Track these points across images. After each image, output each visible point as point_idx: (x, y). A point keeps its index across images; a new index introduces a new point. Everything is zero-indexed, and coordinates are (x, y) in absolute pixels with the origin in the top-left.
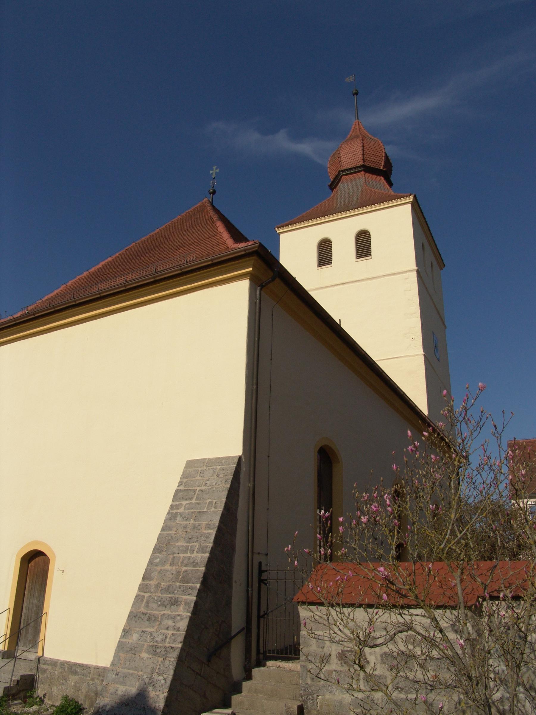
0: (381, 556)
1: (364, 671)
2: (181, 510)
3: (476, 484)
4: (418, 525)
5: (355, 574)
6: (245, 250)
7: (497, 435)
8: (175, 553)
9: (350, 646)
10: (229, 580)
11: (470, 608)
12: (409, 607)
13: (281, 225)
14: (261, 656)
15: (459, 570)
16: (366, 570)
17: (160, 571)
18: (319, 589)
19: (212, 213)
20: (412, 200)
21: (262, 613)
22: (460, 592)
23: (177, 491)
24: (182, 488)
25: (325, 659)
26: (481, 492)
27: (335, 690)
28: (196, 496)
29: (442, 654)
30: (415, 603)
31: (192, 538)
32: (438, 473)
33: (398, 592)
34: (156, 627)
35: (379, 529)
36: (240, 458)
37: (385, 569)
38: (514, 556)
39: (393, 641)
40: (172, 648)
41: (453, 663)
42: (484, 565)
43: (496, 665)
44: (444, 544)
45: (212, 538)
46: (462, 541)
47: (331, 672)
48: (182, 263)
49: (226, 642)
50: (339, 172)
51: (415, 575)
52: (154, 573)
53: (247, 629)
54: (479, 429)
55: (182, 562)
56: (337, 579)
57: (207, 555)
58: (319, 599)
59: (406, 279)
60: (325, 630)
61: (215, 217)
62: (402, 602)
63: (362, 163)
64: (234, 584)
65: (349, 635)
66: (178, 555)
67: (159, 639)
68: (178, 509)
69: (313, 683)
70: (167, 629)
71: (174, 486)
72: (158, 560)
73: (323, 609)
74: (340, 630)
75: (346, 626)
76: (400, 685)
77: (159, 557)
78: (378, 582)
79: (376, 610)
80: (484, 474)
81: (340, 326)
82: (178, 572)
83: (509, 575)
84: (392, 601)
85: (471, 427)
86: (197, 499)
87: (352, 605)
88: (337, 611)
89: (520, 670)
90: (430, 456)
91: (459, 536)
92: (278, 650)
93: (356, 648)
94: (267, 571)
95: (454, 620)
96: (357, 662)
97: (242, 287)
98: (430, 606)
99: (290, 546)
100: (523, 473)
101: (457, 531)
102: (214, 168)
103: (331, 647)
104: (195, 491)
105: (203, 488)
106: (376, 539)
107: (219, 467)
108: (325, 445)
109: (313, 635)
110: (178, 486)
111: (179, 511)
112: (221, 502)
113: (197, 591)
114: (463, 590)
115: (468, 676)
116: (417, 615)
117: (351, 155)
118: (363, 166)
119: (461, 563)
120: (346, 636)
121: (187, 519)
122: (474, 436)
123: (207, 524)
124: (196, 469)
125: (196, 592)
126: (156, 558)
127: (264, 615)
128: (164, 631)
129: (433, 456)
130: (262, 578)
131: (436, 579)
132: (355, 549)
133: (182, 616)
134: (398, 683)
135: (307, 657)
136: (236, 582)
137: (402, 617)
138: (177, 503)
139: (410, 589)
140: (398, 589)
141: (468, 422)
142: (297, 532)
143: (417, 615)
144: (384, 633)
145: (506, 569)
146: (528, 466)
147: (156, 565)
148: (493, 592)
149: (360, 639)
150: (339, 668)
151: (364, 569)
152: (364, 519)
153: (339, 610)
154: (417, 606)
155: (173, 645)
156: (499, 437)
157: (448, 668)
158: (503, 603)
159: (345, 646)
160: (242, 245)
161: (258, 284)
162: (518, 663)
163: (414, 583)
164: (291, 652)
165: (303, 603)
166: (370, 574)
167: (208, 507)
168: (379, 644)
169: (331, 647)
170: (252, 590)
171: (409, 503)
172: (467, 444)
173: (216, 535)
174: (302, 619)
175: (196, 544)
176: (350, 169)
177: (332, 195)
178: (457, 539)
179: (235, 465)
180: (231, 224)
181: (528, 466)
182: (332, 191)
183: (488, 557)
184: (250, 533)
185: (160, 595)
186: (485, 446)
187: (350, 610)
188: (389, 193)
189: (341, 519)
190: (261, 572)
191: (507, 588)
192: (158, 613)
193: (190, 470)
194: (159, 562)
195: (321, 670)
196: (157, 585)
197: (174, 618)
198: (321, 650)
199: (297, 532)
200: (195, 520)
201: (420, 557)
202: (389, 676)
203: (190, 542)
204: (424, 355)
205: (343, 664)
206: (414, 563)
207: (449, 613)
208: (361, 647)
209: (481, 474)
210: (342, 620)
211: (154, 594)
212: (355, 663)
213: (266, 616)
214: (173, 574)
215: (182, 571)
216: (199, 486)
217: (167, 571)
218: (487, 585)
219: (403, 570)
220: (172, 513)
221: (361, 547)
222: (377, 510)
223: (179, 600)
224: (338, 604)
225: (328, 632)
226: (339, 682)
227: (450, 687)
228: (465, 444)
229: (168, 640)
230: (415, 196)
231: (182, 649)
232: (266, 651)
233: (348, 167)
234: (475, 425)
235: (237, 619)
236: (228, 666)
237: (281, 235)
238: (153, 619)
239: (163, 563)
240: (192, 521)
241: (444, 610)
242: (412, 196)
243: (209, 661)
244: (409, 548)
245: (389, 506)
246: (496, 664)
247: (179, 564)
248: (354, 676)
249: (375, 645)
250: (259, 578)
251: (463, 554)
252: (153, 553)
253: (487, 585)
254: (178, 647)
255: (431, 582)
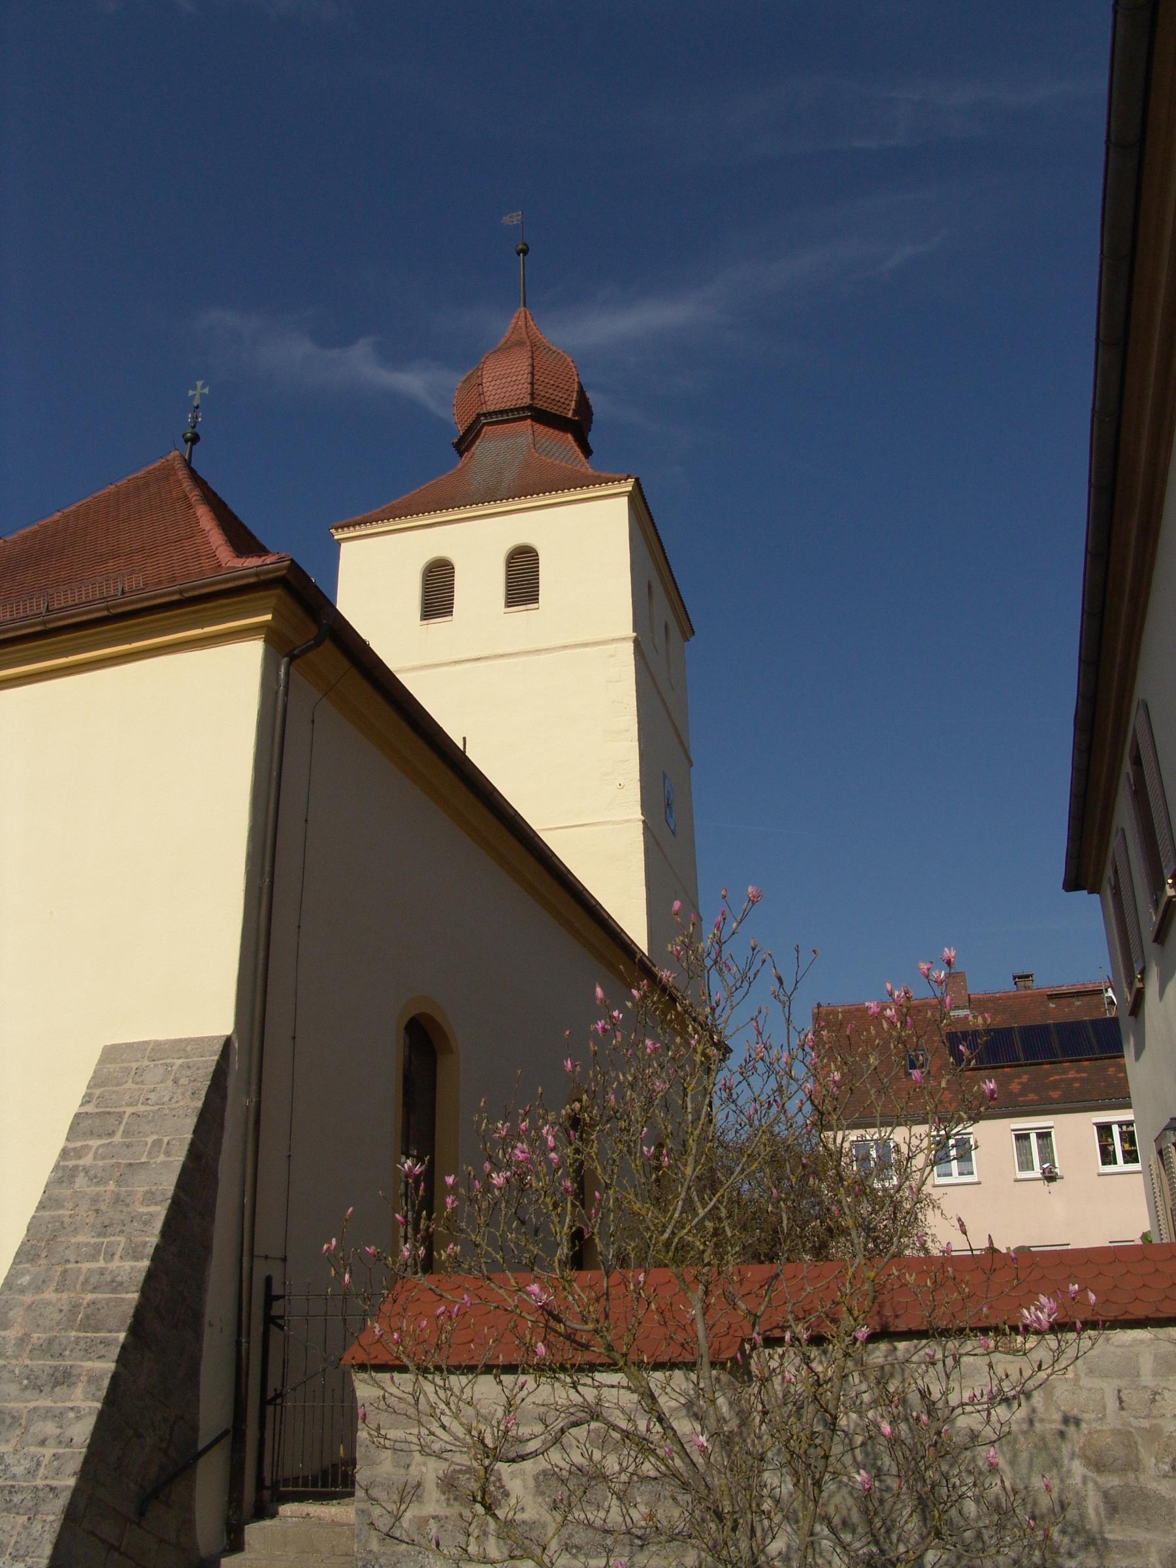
0: (534, 1261)
1: (494, 1516)
2: (87, 1160)
3: (739, 1103)
4: (615, 1192)
5: (478, 1301)
6: (257, 574)
7: (783, 998)
8: (68, 1261)
9: (463, 1460)
10: (194, 1320)
11: (723, 1365)
12: (592, 1368)
13: (342, 523)
14: (267, 1494)
15: (701, 1287)
16: (501, 1291)
17: (30, 1306)
18: (396, 1336)
19: (187, 485)
20: (630, 489)
21: (271, 1394)
22: (701, 1334)
23: (77, 1116)
24: (90, 1108)
25: (411, 1492)
26: (749, 1118)
27: (432, 1561)
28: (122, 1128)
29: (663, 1468)
30: (606, 1360)
31: (111, 1225)
32: (659, 1077)
33: (570, 1337)
34: (13, 1442)
35: (530, 1202)
36: (228, 1041)
37: (541, 1289)
38: (820, 1251)
39: (558, 1445)
40: (52, 1489)
41: (685, 1486)
42: (756, 1273)
43: (776, 1482)
44: (668, 1231)
45: (158, 1224)
46: (709, 1225)
47: (425, 1521)
48: (112, 593)
49: (182, 1465)
50: (479, 415)
51: (607, 1299)
52: (15, 1311)
53: (236, 1433)
54: (746, 984)
55: (86, 1281)
56: (439, 1312)
57: (146, 1263)
58: (398, 1358)
59: (612, 656)
60: (411, 1427)
61: (194, 495)
62: (580, 1358)
63: (527, 401)
64: (207, 1331)
65: (461, 1435)
66: (75, 1265)
67: (19, 1470)
68: (80, 1158)
69: (383, 1549)
70: (43, 1443)
71: (73, 1105)
72: (26, 1279)
73: (405, 1381)
74: (443, 1427)
75: (456, 1417)
76: (576, 1540)
77: (28, 1271)
78: (528, 1317)
79: (522, 1378)
80: (755, 1080)
81: (464, 753)
82: (75, 1307)
83: (804, 1294)
84: (558, 1358)
85: (731, 982)
86: (126, 1133)
87: (471, 1369)
88: (436, 1385)
89: (821, 1492)
90: (643, 1042)
91: (701, 1212)
92: (305, 1478)
93: (475, 1464)
94: (283, 1297)
95: (692, 1392)
96: (479, 1499)
97: (249, 655)
98: (640, 1365)
99: (334, 1241)
100: (837, 1078)
101: (698, 1204)
102: (199, 384)
103: (425, 1464)
104: (121, 1115)
105: (141, 1108)
106: (523, 1223)
107: (179, 1062)
108: (421, 1015)
109: (382, 1441)
110: (82, 1105)
111: (81, 1162)
112: (181, 1140)
113: (119, 1349)
114: (709, 1328)
115: (714, 1511)
116: (613, 1386)
117: (505, 382)
118: (530, 408)
119: (705, 1270)
120: (457, 1439)
121: (101, 1181)
122: (735, 1000)
123: (147, 1192)
124: (125, 1065)
125: (117, 1351)
126: (23, 1274)
127: (274, 1399)
128: (32, 1449)
129: (648, 1042)
130: (274, 1313)
131: (653, 1306)
132: (477, 1246)
133: (82, 1408)
134: (571, 1536)
135: (367, 1490)
136: (211, 1325)
137: (577, 1391)
138: (79, 1144)
139: (596, 1331)
140: (569, 1331)
141: (724, 969)
142: (351, 1209)
143: (613, 1386)
144: (538, 1428)
145: (800, 1279)
146: (846, 1063)
147: (22, 1291)
148: (770, 1330)
149: (485, 1446)
150: (442, 1511)
151: (497, 1289)
152: (498, 1179)
153: (441, 1383)
154: (612, 1367)
155: (54, 1483)
156: (787, 1004)
157: (674, 1499)
158: (792, 1351)
159: (453, 1462)
160: (252, 562)
161: (283, 652)
162: (817, 1476)
163: (607, 1317)
164: (334, 1480)
165: (363, 1367)
166: (510, 1300)
167: (150, 1153)
168: (527, 1455)
169: (425, 1464)
170: (248, 1342)
171: (595, 1145)
172: (720, 1016)
173: (167, 1216)
174: (359, 1404)
175: (118, 1239)
176: (501, 412)
177: (460, 465)
178: (696, 1220)
179: (216, 1058)
180: (231, 514)
181: (846, 1063)
182: (461, 456)
183: (766, 1255)
184: (247, 1212)
185: (28, 1362)
186: (760, 1020)
187: (464, 1379)
188: (583, 470)
189: (450, 1180)
190: (270, 1298)
191: (797, 1319)
192: (21, 1405)
193: (112, 1067)
194: (30, 1284)
195: (398, 1518)
196: (22, 1340)
197: (58, 1416)
198: (403, 1471)
199: (351, 1209)
200: (118, 1183)
201: (623, 1261)
202: (551, 1520)
203: (105, 1235)
204: (644, 822)
205: (452, 1501)
206: (608, 1274)
207: (683, 1377)
208: (487, 1462)
209: (750, 1079)
210: (447, 1404)
211: (14, 1362)
212: (475, 1500)
213: (279, 1401)
214: (61, 1311)
215: (85, 1302)
216: (130, 1105)
217: (49, 1303)
218: (759, 1317)
219: (581, 1291)
220: (64, 1167)
221: (492, 1241)
222: (527, 1159)
223: (75, 1372)
224: (438, 1369)
225: (415, 1431)
226: (438, 1545)
227: (680, 1537)
228: (716, 1016)
229: (42, 1470)
230: (637, 480)
231: (76, 1491)
232: (277, 1482)
233: (498, 408)
234: (738, 976)
235: (212, 1414)
236: (187, 1524)
237: (344, 546)
238: (9, 1421)
239: (38, 1286)
240: (112, 1186)
241: (668, 1373)
242: (631, 481)
243: (142, 1513)
244: (597, 1240)
245: (553, 1149)
246: (778, 1482)
247: (78, 1286)
248: (471, 1530)
249: (519, 1456)
250: (263, 1312)
251: (709, 1251)
252: (14, 1263)
253: (759, 1317)
254: (67, 1487)
255: (641, 1312)
